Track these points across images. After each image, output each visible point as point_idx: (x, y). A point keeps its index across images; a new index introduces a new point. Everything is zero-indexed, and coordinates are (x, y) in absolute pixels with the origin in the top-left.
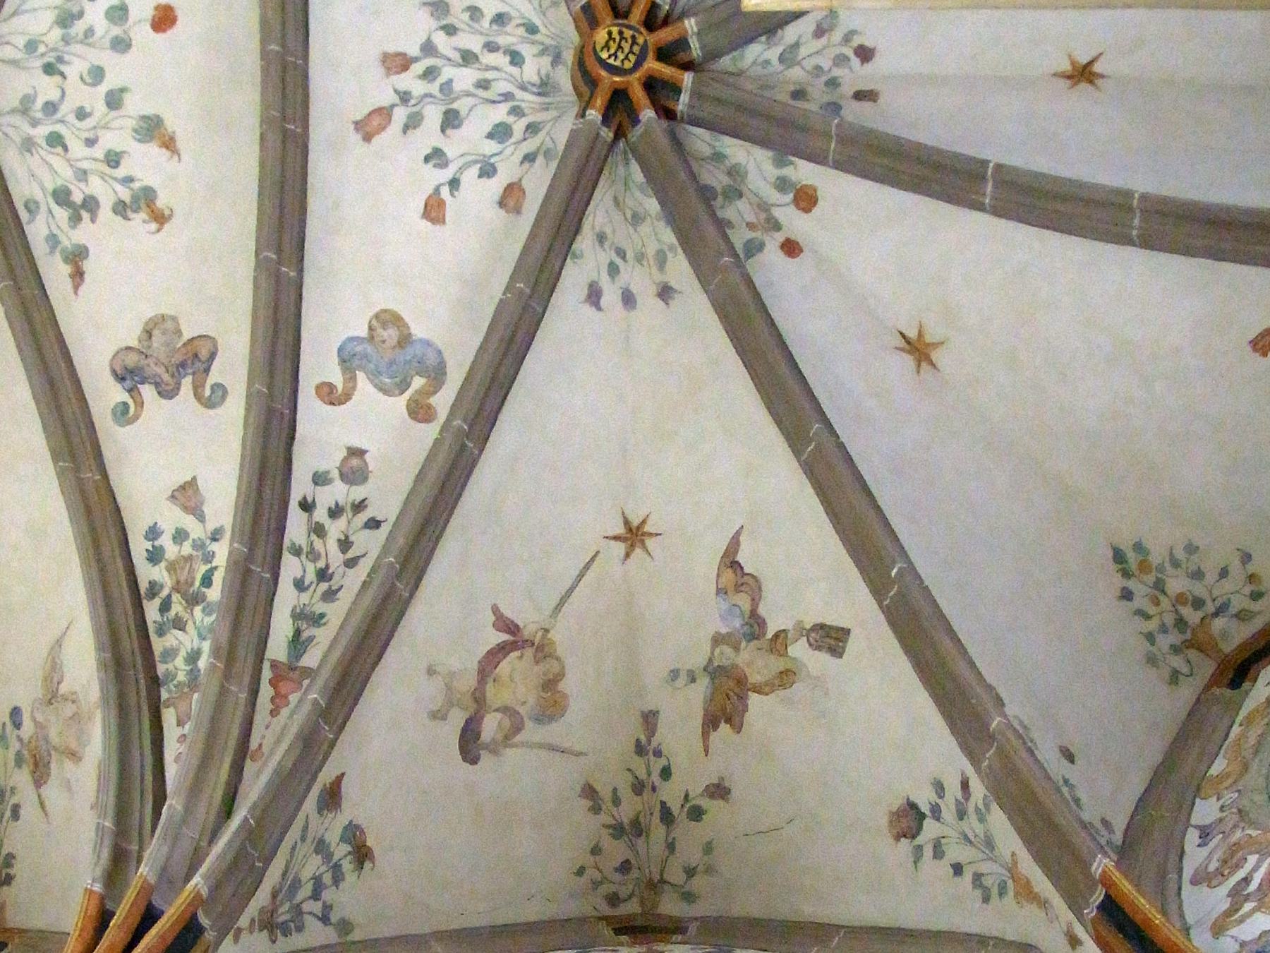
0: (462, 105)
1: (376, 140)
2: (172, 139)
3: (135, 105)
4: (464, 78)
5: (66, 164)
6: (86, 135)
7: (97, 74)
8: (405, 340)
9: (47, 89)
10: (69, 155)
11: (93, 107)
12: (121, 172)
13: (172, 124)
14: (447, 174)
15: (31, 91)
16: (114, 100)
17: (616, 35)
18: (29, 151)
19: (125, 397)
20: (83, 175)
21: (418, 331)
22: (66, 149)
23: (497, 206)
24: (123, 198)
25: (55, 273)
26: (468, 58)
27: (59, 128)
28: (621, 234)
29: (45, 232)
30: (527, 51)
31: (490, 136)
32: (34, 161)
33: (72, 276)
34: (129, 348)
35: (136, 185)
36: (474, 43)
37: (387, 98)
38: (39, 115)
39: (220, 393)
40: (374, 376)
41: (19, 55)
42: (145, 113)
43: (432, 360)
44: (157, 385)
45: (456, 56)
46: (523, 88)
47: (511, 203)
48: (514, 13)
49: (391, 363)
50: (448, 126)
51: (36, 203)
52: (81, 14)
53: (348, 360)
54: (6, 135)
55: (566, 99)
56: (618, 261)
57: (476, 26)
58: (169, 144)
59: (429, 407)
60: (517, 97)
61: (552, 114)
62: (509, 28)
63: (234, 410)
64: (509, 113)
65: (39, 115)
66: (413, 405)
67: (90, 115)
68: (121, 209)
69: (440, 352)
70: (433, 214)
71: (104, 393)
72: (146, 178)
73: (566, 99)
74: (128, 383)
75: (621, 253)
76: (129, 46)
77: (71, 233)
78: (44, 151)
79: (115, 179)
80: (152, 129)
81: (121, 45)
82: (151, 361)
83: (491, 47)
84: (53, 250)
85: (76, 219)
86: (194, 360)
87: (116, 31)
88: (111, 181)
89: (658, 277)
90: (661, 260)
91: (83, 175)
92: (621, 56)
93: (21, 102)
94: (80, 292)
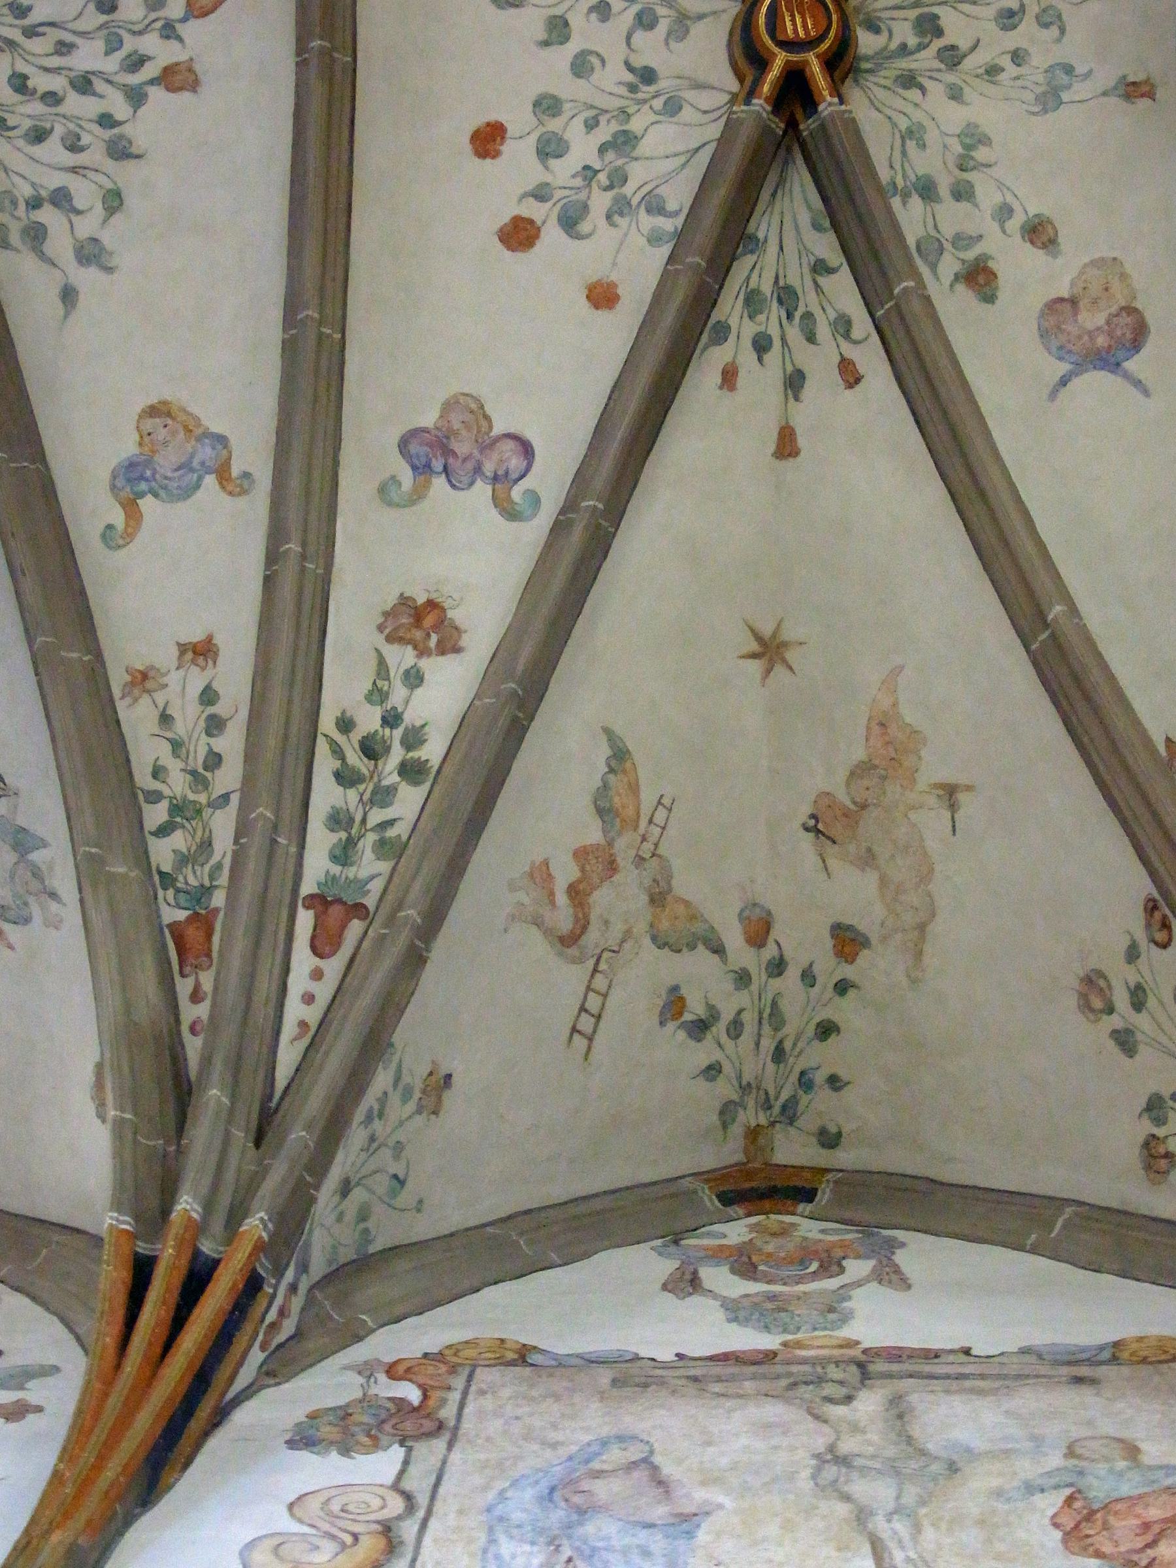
4: (89, 57)
7: (581, 66)
9: (650, 48)
26: (84, 84)
36: (75, 103)
37: (191, 30)
41: (689, 95)
42: (512, 11)
45: (99, 86)
48: (21, 143)
52: (602, 149)
62: (27, 124)
76: (537, 104)
83: (52, 98)
87: (554, 125)
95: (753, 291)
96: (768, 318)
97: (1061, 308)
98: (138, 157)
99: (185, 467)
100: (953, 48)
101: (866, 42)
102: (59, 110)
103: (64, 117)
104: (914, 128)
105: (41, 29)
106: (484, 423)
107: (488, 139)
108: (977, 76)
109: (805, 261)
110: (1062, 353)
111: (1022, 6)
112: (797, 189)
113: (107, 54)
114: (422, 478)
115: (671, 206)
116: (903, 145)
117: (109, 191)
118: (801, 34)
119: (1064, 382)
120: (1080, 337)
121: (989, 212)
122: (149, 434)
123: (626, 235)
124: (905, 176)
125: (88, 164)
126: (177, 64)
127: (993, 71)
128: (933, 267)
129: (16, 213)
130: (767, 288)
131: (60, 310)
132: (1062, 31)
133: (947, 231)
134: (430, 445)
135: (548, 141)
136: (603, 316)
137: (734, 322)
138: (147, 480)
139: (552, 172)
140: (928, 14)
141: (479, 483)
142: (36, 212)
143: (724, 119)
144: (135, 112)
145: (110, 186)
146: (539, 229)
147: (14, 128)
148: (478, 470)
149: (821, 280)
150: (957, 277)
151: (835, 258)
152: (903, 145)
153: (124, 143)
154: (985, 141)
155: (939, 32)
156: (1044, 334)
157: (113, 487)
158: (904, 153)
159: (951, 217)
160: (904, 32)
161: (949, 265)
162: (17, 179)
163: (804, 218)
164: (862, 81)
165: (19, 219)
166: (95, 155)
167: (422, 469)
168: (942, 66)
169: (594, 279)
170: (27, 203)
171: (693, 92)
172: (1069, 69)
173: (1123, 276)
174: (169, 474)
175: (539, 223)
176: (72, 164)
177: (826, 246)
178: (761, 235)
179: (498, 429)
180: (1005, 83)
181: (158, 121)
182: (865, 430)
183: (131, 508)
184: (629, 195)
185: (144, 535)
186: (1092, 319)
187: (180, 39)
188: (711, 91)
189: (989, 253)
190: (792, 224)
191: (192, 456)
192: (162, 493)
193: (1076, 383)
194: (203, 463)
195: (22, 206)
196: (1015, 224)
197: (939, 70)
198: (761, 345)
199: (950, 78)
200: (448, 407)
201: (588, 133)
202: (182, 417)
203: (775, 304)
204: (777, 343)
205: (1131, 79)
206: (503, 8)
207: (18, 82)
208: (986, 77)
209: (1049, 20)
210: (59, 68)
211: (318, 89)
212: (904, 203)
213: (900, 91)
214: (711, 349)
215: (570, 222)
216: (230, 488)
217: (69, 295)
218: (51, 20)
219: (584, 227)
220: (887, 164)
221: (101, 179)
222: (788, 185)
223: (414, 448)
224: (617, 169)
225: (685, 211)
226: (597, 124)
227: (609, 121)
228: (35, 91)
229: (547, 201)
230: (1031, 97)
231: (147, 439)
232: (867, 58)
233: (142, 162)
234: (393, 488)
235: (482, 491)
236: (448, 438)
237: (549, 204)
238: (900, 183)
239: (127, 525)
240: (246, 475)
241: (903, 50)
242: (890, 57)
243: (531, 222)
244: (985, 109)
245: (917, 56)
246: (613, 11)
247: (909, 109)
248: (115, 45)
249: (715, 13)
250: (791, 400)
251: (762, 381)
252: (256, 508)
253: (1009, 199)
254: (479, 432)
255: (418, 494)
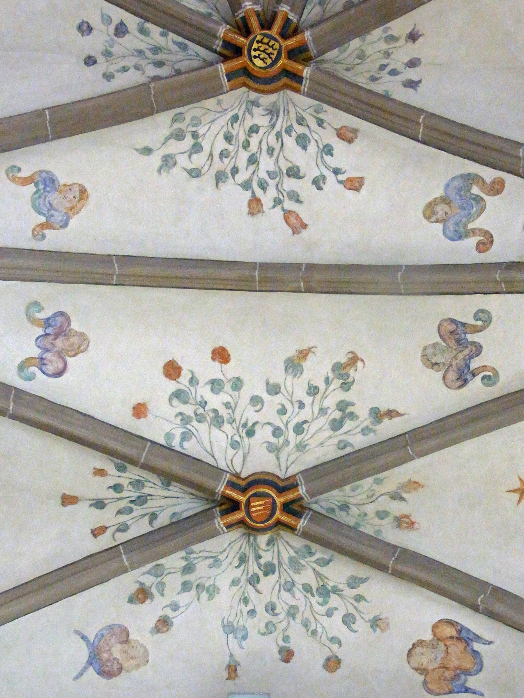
0: (284, 166)
1: (305, 221)
2: (301, 352)
3: (278, 376)
4: (266, 163)
5: (316, 421)
6: (296, 409)
7: (256, 400)
8: (445, 200)
9: (264, 434)
10: (310, 420)
11: (278, 404)
12: (322, 386)
13: (292, 352)
14: (330, 177)
15: (265, 445)
16: (274, 389)
17: (257, 53)
18: (305, 447)
19: (478, 378)
20: (323, 411)
21: (439, 192)
22: (306, 422)
23: (352, 145)
24: (339, 385)
25: (389, 429)
26: (253, 160)
27: (291, 426)
28: (371, 65)
29: (360, 437)
30: (249, 123)
31: (305, 148)
32: (313, 443)
33: (391, 418)
34: (444, 378)
35: (331, 376)
36: (244, 156)
37: (278, 212)
38: (281, 440)
39: (481, 314)
40: (471, 218)
41: (240, 453)
42: (284, 368)
43: (460, 183)
44: (471, 358)
45: (252, 168)
46: (273, 126)
47: (350, 135)
48: (225, 129)
49: (462, 208)
50: (298, 175)
51: (340, 442)
52: (215, 411)
53: (460, 235)
54: (292, 463)
55: (281, 100)
56: (388, 69)
57: (232, 154)
58: (304, 354)
59: (493, 182)
60: (279, 130)
61: (291, 108)
62: (234, 133)
63: (493, 303)
64: (290, 135)
65: (281, 440)
66: (492, 192)
67: (283, 406)
68: (346, 386)
69: (453, 179)
70: (357, 184)
71: (476, 392)
72: (327, 369)
73: (281, 100)
74: (469, 377)
75: (383, 67)
76: (238, 379)
77: (361, 419)
78: (305, 437)
79: (326, 390)
80: (294, 365)
81: (237, 384)
82: (454, 363)
83: (246, 145)
84: (371, 430)
85: (352, 416)
86: (456, 334)
87: (228, 387)
88: (327, 393)
89: (402, 41)
90: (392, 39)
91: (323, 411)
92: (270, 50)
93: (271, 452)
94: (403, 412)
95: (143, 484)
96: (131, 491)
97: (124, 636)
98: (217, 186)
99: (51, 207)
100: (258, 581)
101: (263, 539)
102: (241, 149)
103: (238, 150)
104: (219, 563)
105: (280, 140)
106: (73, 353)
107: (221, 355)
108: (244, 593)
109: (158, 509)
110: (100, 636)
111: (277, 614)
112: (195, 505)
113: (267, 172)
114: (43, 323)
115: (186, 444)
116: (211, 557)
117: (200, 171)
118: (254, 509)
119: (84, 638)
120: (108, 645)
121: (175, 599)
122: (70, 190)
123: (171, 422)
124: (196, 558)
125: (214, 161)
126: (262, 205)
127: (246, 601)
128: (149, 573)
129: (190, 126)
130: (146, 490)
131: (139, 147)
132: (264, 634)
133: (167, 579)
134: (61, 327)
135: (220, 385)
136: (129, 411)
137: (127, 475)
138: (44, 188)
139: (203, 387)
140: (275, 569)
141: (39, 351)
142: (190, 136)
143: (228, 470)
144: (239, 185)
145: (203, 172)
146: (175, 380)
147: (232, 126)
148: (47, 350)
149: (147, 517)
150: (142, 584)
151: (158, 524)
152: (211, 557)
153: (224, 179)
154: (211, 597)
155: (266, 574)
156: (110, 627)
157: (41, 172)
158: (207, 558)
159: (173, 582)
160: (267, 557)
161: (149, 580)
162: (207, 127)
163: (178, 509)
164: (244, 537)
165: (187, 127)
166: (218, 165)
167: (47, 323)
168: (249, 576)
169: (149, 407)
170: (195, 132)
171: (242, 455)
172: (244, 638)
173: (138, 666)
174: (47, 199)
175: (178, 380)
176: (214, 153)
177: (163, 520)
178: (171, 488)
179: (69, 360)
180: (239, 607)
181: (234, 196)
182: (73, 537)
183: (26, 181)
184: (192, 423)
185: (13, 186)
186: (117, 651)
187: (274, 207)
188: (242, 463)
189: (154, 601)
190: (174, 503)
191: (57, 211)
192: (37, 196)
193: (84, 644)
194: (52, 215)
195: (194, 129)
196: (169, 612)
197: (247, 575)
198: (117, 488)
199: (244, 579)
200: (83, 337)
201: (223, 404)
202: (79, 206)
203: (138, 494)
204: (119, 495)
205: (238, 668)
206: (285, 363)
207: (255, 128)
208: (243, 598)
209: (269, 627)
210: (261, 149)
211: (235, 274)
212: (182, 558)
213: (238, 555)
214: (113, 464)
215: (178, 395)
216: (37, 229)
217: (147, 151)
218: (284, 144)
219: (175, 402)
220: (202, 549)
221: (206, 167)
222: (196, 501)
223: (59, 319)
224: (205, 417)
225: (183, 451)
226: (228, 408)
227: (229, 414)
228: (250, 137)
229: (190, 383)
230: (231, 619)
231: (68, 188)
232: (255, 540)
233: (214, 187)
234: (37, 309)
235: (36, 352)
236: (65, 335)
237: (188, 385)
238: (192, 556)
239: (19, 178)
240: (44, 237)
241: (259, 557)
242: (255, 549)
243: (179, 375)
244: (227, 596)
245: (255, 563)
246: (282, 416)
247: (229, 559)
248: (272, 175)
249: (280, 466)
250: (91, 502)
251: (100, 488)
252: (26, 242)
253: (181, 610)
254: (68, 351)
255: (33, 321)
